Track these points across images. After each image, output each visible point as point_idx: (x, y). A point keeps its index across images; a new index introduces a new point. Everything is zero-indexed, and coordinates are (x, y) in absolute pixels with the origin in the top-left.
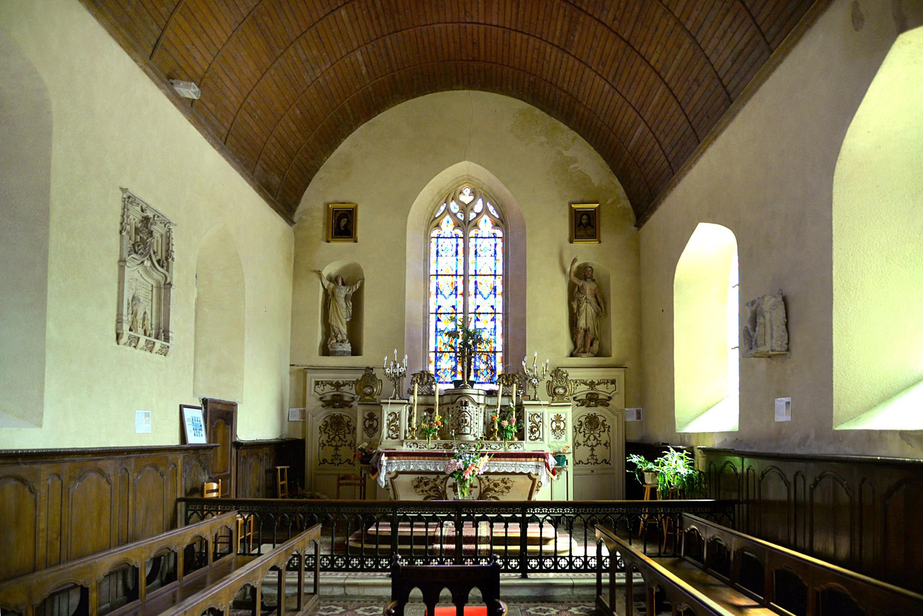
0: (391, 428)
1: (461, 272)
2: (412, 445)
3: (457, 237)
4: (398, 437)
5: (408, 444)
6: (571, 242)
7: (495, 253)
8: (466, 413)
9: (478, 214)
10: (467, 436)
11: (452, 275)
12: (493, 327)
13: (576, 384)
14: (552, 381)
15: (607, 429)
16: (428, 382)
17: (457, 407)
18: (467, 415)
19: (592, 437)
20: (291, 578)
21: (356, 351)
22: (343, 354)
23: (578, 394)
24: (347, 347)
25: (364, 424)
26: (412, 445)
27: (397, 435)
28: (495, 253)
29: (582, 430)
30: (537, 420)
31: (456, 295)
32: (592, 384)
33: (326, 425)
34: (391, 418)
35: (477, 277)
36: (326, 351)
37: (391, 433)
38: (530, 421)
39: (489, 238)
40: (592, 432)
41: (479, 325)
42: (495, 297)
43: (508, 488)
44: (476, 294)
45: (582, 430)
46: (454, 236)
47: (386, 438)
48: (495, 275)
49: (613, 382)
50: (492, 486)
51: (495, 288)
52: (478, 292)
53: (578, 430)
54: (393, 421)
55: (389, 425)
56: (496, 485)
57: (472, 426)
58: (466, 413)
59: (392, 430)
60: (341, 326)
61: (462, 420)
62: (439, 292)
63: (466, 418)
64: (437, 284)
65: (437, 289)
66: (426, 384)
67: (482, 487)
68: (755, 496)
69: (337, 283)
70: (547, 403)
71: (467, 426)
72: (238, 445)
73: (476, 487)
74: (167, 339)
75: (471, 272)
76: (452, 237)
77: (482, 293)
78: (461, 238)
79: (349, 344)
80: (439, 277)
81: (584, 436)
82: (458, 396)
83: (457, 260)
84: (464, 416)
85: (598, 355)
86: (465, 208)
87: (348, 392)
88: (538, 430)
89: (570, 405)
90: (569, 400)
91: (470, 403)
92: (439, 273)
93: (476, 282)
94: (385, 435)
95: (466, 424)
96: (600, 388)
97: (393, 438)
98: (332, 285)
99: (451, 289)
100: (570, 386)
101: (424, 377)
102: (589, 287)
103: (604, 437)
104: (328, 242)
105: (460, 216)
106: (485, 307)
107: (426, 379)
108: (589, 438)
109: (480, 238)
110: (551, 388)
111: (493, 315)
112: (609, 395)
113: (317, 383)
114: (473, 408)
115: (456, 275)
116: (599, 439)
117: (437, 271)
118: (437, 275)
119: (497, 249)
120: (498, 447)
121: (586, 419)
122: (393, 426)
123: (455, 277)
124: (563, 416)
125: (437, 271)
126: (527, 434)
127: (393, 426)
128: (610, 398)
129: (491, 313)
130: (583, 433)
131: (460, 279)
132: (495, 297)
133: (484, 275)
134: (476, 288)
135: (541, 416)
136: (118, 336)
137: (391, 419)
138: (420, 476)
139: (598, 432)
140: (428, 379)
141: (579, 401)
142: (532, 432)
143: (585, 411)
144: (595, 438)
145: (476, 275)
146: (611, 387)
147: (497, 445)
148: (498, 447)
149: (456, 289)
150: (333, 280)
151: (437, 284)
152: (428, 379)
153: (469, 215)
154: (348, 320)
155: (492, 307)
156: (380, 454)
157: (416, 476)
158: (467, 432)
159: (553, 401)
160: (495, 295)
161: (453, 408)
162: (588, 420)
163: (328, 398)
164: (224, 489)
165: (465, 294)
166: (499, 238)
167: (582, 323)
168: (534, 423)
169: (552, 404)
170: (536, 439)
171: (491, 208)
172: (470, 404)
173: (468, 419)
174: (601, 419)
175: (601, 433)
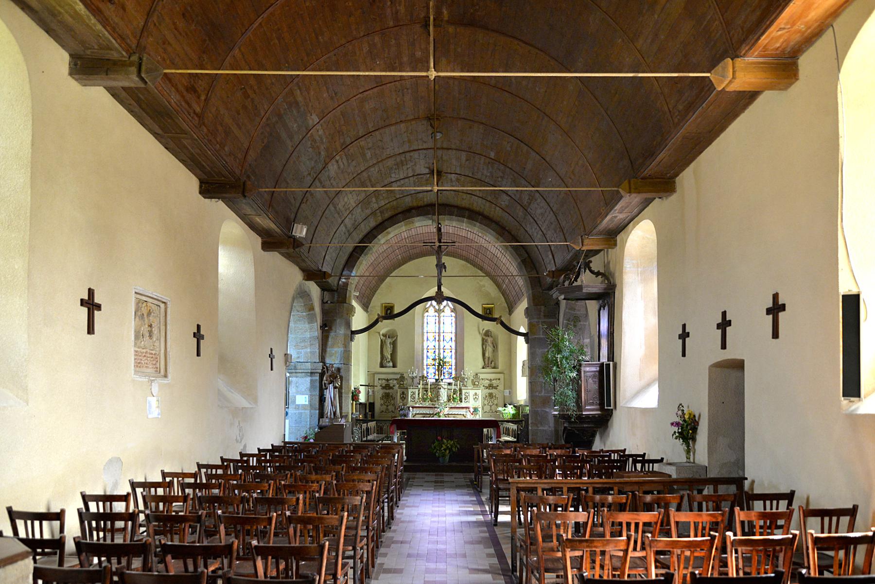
1: (437, 331)
21: (394, 366)
22: (390, 367)
24: (391, 364)
36: (382, 366)
49: (499, 379)
60: (388, 354)
75: (441, 331)
113: (379, 379)
126: (463, 400)
143: (488, 391)
150: (385, 335)
165: (439, 341)
174: (494, 394)
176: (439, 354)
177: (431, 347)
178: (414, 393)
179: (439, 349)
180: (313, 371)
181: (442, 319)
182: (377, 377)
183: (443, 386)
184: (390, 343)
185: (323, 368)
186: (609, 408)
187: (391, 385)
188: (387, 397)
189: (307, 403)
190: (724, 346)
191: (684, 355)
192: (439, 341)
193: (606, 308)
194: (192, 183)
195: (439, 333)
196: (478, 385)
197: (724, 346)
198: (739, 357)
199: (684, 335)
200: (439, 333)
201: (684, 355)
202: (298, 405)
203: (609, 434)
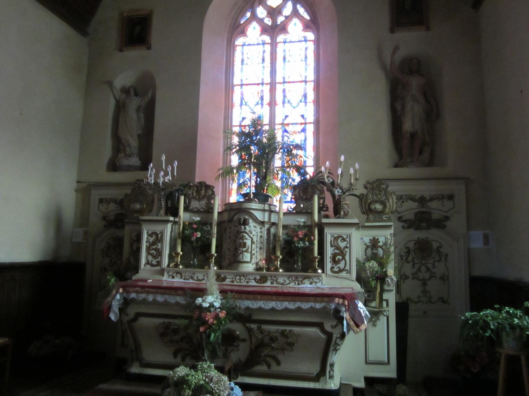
0: (151, 252)
1: (268, 80)
2: (175, 275)
3: (264, 44)
4: (159, 264)
5: (171, 273)
6: (392, 31)
7: (306, 57)
8: (245, 235)
9: (287, 17)
10: (246, 265)
11: (258, 84)
12: (303, 139)
13: (401, 201)
14: (367, 194)
15: (443, 258)
16: (205, 195)
17: (235, 226)
18: (247, 236)
19: (423, 269)
23: (403, 214)
24: (135, 161)
25: (366, 253)
26: (175, 275)
27: (158, 262)
28: (306, 57)
29: (410, 259)
30: (342, 245)
31: (262, 104)
32: (422, 200)
33: (408, 252)
34: (151, 240)
35: (286, 85)
36: (113, 166)
37: (150, 258)
38: (332, 246)
39: (299, 41)
40: (424, 262)
42: (306, 105)
43: (291, 345)
44: (284, 103)
45: (410, 259)
46: (261, 43)
47: (145, 265)
48: (306, 82)
49: (451, 197)
50: (267, 340)
51: (305, 96)
52: (287, 101)
53: (404, 258)
54: (154, 243)
55: (148, 249)
56: (273, 339)
57: (253, 252)
58: (245, 235)
59: (151, 254)
61: (240, 243)
62: (244, 103)
63: (245, 241)
64: (242, 94)
65: (242, 99)
66: (203, 198)
67: (254, 340)
69: (130, 93)
70: (356, 221)
71: (246, 251)
73: (244, 340)
75: (279, 79)
76: (259, 44)
77: (291, 101)
78: (268, 44)
79: (138, 158)
80: (244, 87)
81: (413, 267)
82: (235, 212)
83: (264, 67)
84: (243, 238)
85: (430, 163)
86: (273, 12)
88: (344, 258)
89: (390, 226)
90: (389, 220)
91: (251, 221)
92: (244, 83)
93: (284, 91)
94: (143, 261)
95: (244, 249)
96: (434, 205)
97: (152, 265)
98: (124, 96)
99: (257, 99)
100: (391, 201)
101: (201, 190)
102: (415, 82)
103: (440, 269)
104: (121, 50)
105: (268, 21)
106: (294, 117)
107: (203, 192)
108: (419, 270)
109: (289, 42)
110: (365, 205)
111: (303, 126)
112: (445, 214)
113: (101, 201)
114: (255, 227)
115: (262, 84)
116: (434, 270)
117: (242, 80)
118: (242, 85)
119: (307, 53)
120: (288, 281)
121: (415, 244)
122: (153, 249)
123: (261, 86)
124: (382, 240)
125: (242, 80)
126: (329, 265)
127: (153, 249)
128: (447, 218)
129: (301, 124)
130: (411, 264)
131: (267, 88)
132: (306, 105)
133: (294, 82)
134: (285, 96)
135: (348, 239)
137: (151, 241)
138: (167, 321)
139: (431, 261)
140: (206, 192)
141: (405, 221)
142: (334, 261)
143: (415, 235)
144: (428, 269)
145: (284, 82)
146: (448, 204)
147: (286, 279)
148: (288, 281)
149: (262, 98)
150: (126, 91)
151: (242, 94)
152: (206, 192)
154: (140, 132)
155: (303, 116)
157: (161, 320)
158: (245, 259)
159: (368, 220)
160: (306, 102)
161: (230, 228)
162: (417, 246)
163: (112, 218)
165: (272, 104)
166: (310, 41)
167: (408, 126)
168: (338, 248)
169: (366, 224)
170: (341, 271)
171: (301, 10)
172: (251, 222)
173: (248, 242)
174: (435, 245)
175: (437, 264)
178: (158, 238)
181: (280, 48)
182: (96, 195)
183: (259, 215)
184: (138, 110)
187: (435, 216)
196: (381, 213)
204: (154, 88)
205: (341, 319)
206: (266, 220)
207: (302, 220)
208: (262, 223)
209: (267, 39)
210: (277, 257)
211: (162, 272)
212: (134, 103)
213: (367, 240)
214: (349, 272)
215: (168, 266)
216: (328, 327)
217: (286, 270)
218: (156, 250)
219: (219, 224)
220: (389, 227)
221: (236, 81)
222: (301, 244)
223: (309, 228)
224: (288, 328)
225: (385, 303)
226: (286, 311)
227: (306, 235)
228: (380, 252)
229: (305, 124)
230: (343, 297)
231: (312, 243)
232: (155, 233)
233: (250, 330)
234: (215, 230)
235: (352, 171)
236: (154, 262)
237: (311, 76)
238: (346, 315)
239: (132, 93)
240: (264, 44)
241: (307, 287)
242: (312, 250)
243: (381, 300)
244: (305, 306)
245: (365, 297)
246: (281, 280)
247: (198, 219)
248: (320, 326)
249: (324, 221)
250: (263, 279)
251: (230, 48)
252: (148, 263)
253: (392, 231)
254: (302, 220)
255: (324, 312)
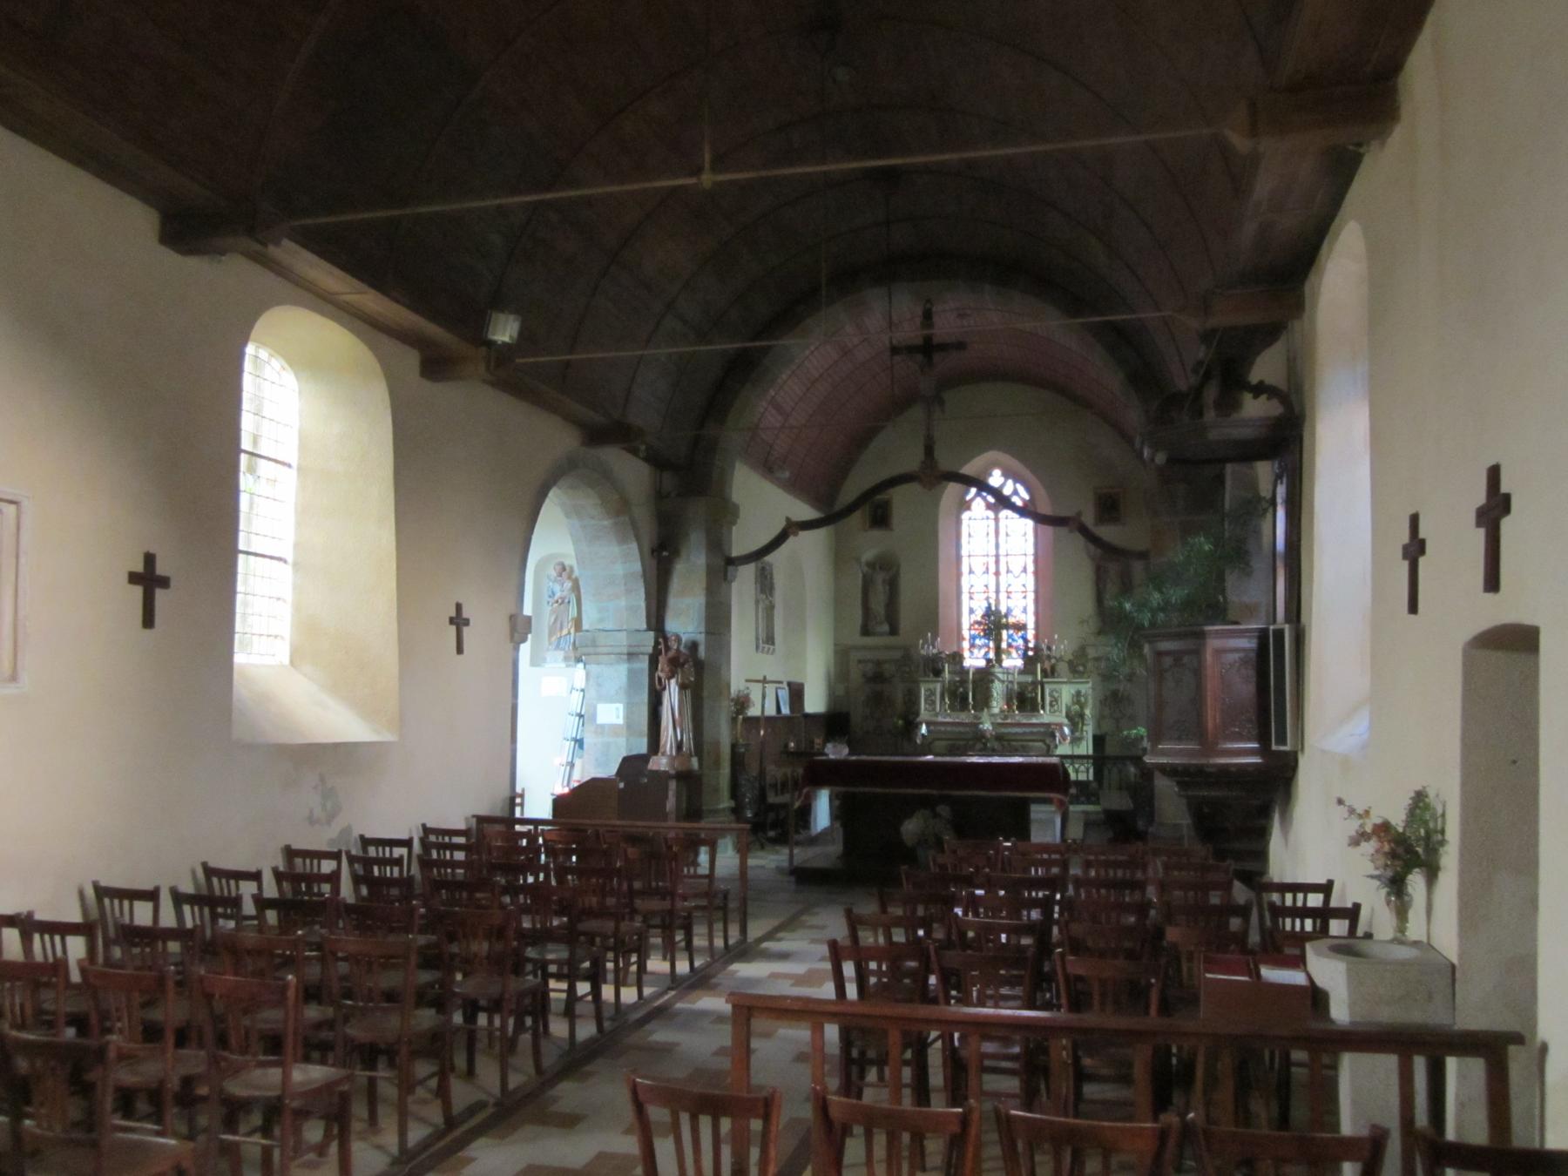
1: (994, 553)
3: (988, 518)
4: (934, 709)
20: (1161, 616)
21: (894, 631)
22: (881, 634)
24: (886, 628)
30: (1056, 695)
34: (928, 693)
36: (866, 631)
37: (927, 706)
41: (1011, 603)
48: (1025, 555)
54: (929, 696)
55: (926, 700)
60: (878, 605)
68: (1087, 750)
70: (1065, 680)
72: (807, 716)
74: (773, 644)
75: (1002, 552)
76: (983, 519)
87: (889, 669)
97: (929, 711)
124: (1083, 692)
126: (1048, 707)
129: (1023, 592)
136: (757, 647)
142: (1051, 705)
149: (987, 568)
150: (871, 565)
153: (912, 1056)
155: (1024, 586)
156: (921, 724)
159: (1074, 678)
164: (797, 745)
165: (997, 573)
170: (1055, 712)
176: (997, 600)
177: (979, 587)
178: (931, 693)
179: (997, 592)
180: (632, 650)
183: (1000, 676)
184: (884, 581)
185: (657, 643)
186: (1282, 748)
188: (878, 700)
189: (621, 721)
190: (1492, 582)
191: (1413, 607)
192: (997, 573)
193: (1285, 480)
194: (139, 220)
195: (997, 556)
197: (1492, 582)
198: (1526, 619)
199: (1415, 549)
200: (997, 556)
201: (1413, 607)
202: (602, 726)
203: (1291, 816)
204: (899, 566)
205: (1054, 737)
206: (1006, 679)
207: (1029, 679)
208: (1003, 682)
209: (991, 514)
210: (946, 703)
211: (937, 715)
212: (880, 577)
213: (1073, 692)
214: (1061, 712)
215: (940, 710)
216: (1048, 741)
217: (1020, 712)
218: (932, 700)
219: (974, 682)
220: (1087, 682)
221: (964, 552)
222: (1029, 695)
223: (1034, 683)
224: (1025, 743)
225: (1085, 733)
226: (1024, 733)
227: (1033, 689)
228: (1083, 699)
229: (1026, 592)
230: (1056, 724)
231: (1037, 694)
232: (930, 690)
233: (1003, 745)
234: (971, 686)
235: (1062, 647)
236: (930, 709)
237: (1031, 550)
238: (1057, 734)
239: (877, 567)
240: (988, 518)
241: (1034, 721)
242: (1036, 699)
243: (1082, 730)
244: (1035, 730)
245: (862, 572)
246: (1017, 718)
247: (958, 679)
248: (1043, 741)
249: (1045, 680)
250: (1006, 717)
251: (959, 522)
252: (926, 709)
253: (1090, 685)
254: (1029, 679)
255: (1044, 734)
